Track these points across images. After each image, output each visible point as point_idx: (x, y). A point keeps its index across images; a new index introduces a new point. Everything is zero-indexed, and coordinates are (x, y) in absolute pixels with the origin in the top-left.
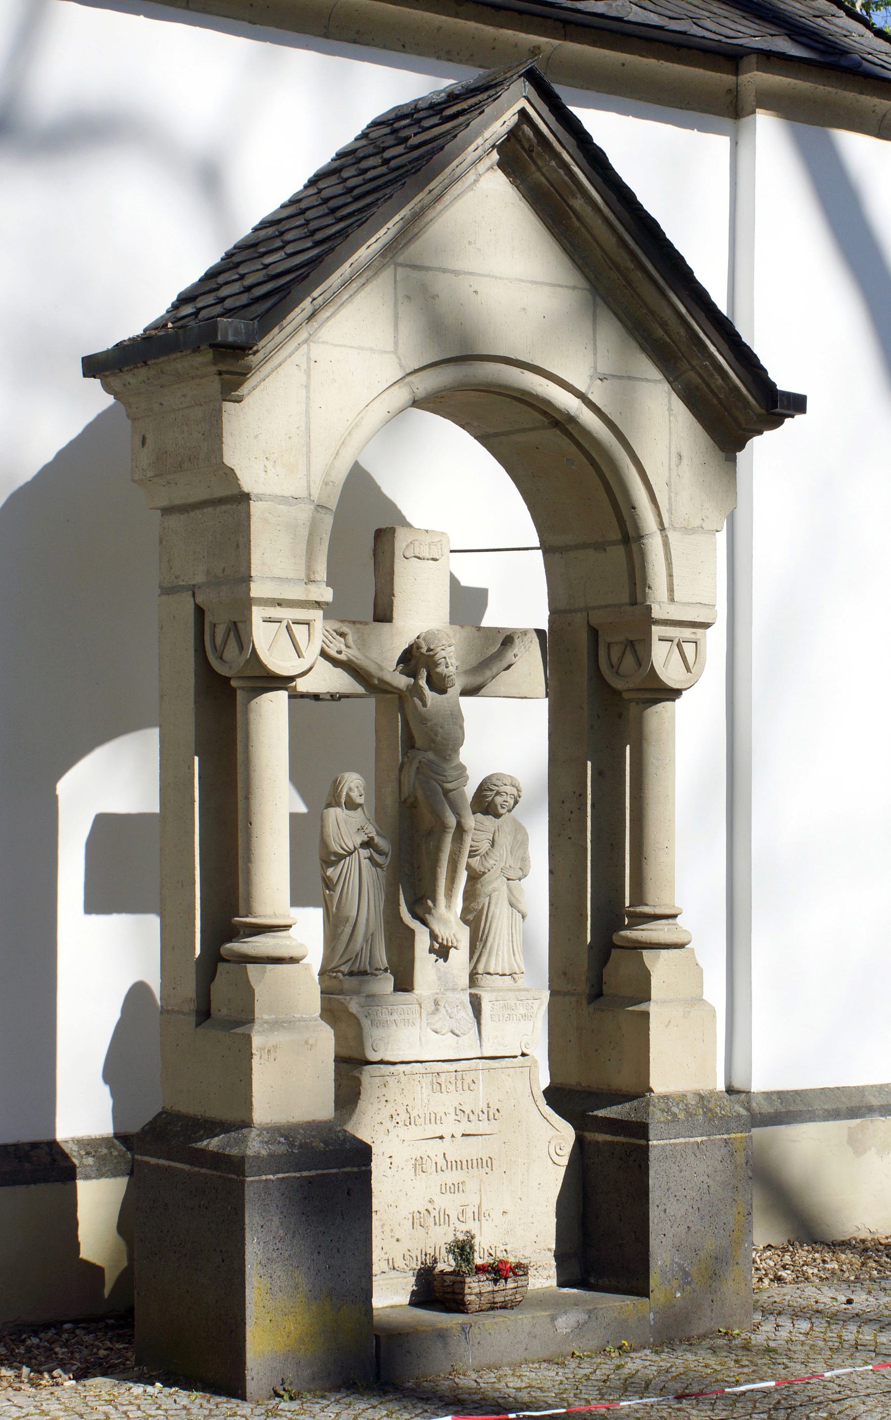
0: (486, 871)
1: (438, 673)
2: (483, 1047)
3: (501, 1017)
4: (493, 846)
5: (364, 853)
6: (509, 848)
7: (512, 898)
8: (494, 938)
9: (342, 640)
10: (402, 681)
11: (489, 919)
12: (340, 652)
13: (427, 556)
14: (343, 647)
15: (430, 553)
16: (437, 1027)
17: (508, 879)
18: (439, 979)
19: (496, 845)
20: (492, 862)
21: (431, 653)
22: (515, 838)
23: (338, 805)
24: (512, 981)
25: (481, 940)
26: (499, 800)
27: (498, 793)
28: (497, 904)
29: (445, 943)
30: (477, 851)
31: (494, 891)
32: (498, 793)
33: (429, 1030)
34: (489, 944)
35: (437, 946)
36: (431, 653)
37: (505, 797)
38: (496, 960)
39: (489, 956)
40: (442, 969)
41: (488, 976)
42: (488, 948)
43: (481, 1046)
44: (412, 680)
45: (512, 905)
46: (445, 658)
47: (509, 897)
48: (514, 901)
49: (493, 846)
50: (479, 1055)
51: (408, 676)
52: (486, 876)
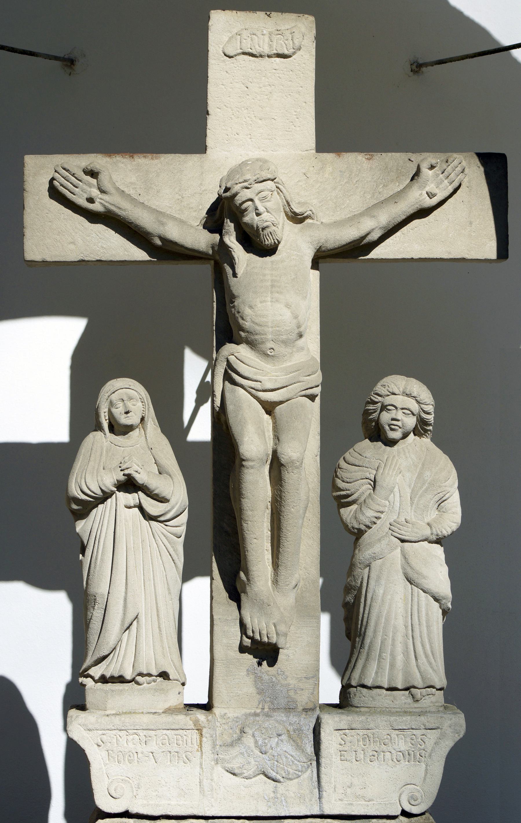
0: (363, 527)
1: (246, 224)
2: (324, 800)
3: (361, 756)
4: (374, 488)
5: (124, 498)
6: (408, 492)
7: (409, 570)
8: (375, 632)
9: (94, 181)
10: (201, 240)
11: (368, 602)
12: (91, 200)
13: (266, 50)
14: (95, 192)
15: (270, 46)
16: (235, 765)
17: (403, 541)
18: (260, 692)
19: (377, 487)
20: (370, 513)
21: (228, 194)
22: (420, 475)
23: (99, 427)
24: (410, 700)
25: (360, 634)
26: (385, 417)
27: (384, 408)
28: (379, 578)
29: (257, 637)
30: (348, 496)
31: (375, 559)
32: (384, 408)
33: (219, 769)
34: (367, 641)
35: (247, 642)
36: (228, 194)
37: (394, 414)
38: (379, 666)
39: (367, 659)
40: (266, 677)
41: (364, 691)
42: (366, 648)
43: (320, 798)
44: (217, 237)
45: (410, 581)
46: (251, 200)
47: (403, 568)
48: (412, 574)
49: (374, 488)
50: (316, 811)
51: (211, 231)
52: (366, 535)
